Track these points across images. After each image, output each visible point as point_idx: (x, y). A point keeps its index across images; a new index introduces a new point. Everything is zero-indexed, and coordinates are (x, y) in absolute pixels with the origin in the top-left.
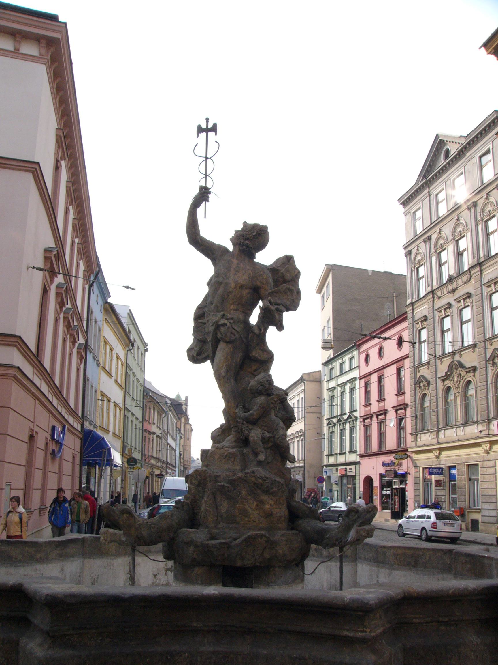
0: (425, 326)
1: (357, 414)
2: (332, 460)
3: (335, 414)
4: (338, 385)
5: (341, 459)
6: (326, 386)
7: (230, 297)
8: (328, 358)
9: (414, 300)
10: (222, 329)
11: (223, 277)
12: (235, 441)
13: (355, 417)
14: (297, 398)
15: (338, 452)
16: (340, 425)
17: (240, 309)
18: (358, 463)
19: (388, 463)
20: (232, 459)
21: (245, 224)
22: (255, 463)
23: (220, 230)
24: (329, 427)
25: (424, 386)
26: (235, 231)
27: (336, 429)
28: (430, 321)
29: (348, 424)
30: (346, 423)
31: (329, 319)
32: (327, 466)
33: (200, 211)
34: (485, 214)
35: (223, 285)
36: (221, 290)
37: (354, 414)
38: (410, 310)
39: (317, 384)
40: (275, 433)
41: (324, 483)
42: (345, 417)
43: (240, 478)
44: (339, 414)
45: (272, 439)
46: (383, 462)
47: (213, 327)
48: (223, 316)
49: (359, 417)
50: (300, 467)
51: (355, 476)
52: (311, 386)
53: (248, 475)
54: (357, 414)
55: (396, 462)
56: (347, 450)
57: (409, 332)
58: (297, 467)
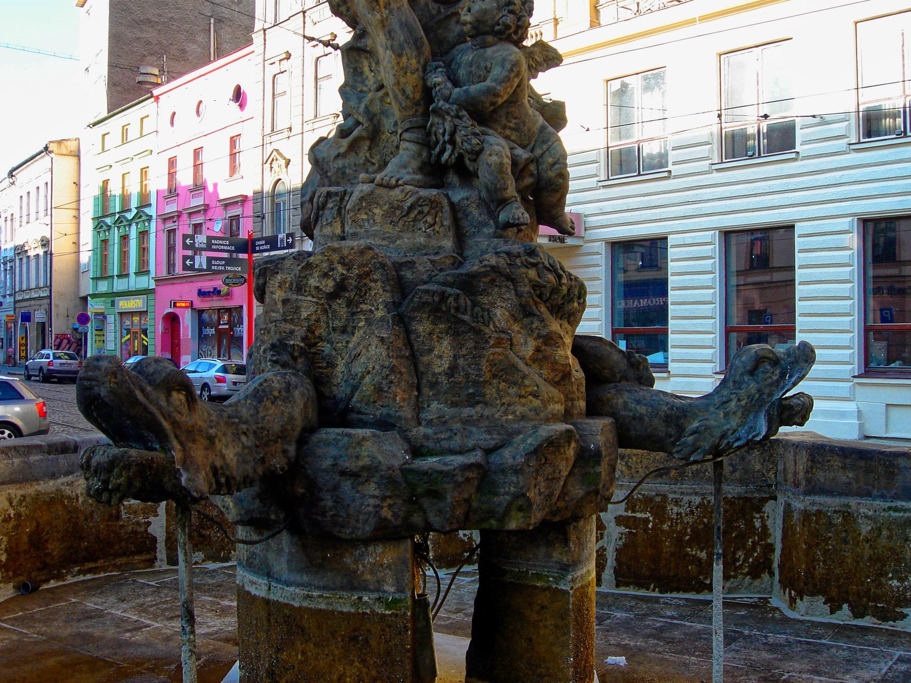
1: (152, 211)
2: (103, 287)
5: (120, 285)
12: (421, 169)
13: (147, 215)
15: (116, 273)
18: (153, 291)
19: (209, 292)
20: (429, 219)
22: (489, 230)
24: (99, 233)
27: (111, 236)
28: (295, 61)
29: (134, 227)
30: (130, 225)
32: (94, 296)
37: (147, 210)
40: (538, 152)
41: (89, 325)
42: (130, 216)
43: (492, 267)
44: (117, 210)
45: (532, 167)
46: (200, 290)
49: (154, 217)
51: (147, 312)
52: (64, 165)
53: (518, 261)
54: (152, 211)
55: (224, 289)
58: (34, 299)
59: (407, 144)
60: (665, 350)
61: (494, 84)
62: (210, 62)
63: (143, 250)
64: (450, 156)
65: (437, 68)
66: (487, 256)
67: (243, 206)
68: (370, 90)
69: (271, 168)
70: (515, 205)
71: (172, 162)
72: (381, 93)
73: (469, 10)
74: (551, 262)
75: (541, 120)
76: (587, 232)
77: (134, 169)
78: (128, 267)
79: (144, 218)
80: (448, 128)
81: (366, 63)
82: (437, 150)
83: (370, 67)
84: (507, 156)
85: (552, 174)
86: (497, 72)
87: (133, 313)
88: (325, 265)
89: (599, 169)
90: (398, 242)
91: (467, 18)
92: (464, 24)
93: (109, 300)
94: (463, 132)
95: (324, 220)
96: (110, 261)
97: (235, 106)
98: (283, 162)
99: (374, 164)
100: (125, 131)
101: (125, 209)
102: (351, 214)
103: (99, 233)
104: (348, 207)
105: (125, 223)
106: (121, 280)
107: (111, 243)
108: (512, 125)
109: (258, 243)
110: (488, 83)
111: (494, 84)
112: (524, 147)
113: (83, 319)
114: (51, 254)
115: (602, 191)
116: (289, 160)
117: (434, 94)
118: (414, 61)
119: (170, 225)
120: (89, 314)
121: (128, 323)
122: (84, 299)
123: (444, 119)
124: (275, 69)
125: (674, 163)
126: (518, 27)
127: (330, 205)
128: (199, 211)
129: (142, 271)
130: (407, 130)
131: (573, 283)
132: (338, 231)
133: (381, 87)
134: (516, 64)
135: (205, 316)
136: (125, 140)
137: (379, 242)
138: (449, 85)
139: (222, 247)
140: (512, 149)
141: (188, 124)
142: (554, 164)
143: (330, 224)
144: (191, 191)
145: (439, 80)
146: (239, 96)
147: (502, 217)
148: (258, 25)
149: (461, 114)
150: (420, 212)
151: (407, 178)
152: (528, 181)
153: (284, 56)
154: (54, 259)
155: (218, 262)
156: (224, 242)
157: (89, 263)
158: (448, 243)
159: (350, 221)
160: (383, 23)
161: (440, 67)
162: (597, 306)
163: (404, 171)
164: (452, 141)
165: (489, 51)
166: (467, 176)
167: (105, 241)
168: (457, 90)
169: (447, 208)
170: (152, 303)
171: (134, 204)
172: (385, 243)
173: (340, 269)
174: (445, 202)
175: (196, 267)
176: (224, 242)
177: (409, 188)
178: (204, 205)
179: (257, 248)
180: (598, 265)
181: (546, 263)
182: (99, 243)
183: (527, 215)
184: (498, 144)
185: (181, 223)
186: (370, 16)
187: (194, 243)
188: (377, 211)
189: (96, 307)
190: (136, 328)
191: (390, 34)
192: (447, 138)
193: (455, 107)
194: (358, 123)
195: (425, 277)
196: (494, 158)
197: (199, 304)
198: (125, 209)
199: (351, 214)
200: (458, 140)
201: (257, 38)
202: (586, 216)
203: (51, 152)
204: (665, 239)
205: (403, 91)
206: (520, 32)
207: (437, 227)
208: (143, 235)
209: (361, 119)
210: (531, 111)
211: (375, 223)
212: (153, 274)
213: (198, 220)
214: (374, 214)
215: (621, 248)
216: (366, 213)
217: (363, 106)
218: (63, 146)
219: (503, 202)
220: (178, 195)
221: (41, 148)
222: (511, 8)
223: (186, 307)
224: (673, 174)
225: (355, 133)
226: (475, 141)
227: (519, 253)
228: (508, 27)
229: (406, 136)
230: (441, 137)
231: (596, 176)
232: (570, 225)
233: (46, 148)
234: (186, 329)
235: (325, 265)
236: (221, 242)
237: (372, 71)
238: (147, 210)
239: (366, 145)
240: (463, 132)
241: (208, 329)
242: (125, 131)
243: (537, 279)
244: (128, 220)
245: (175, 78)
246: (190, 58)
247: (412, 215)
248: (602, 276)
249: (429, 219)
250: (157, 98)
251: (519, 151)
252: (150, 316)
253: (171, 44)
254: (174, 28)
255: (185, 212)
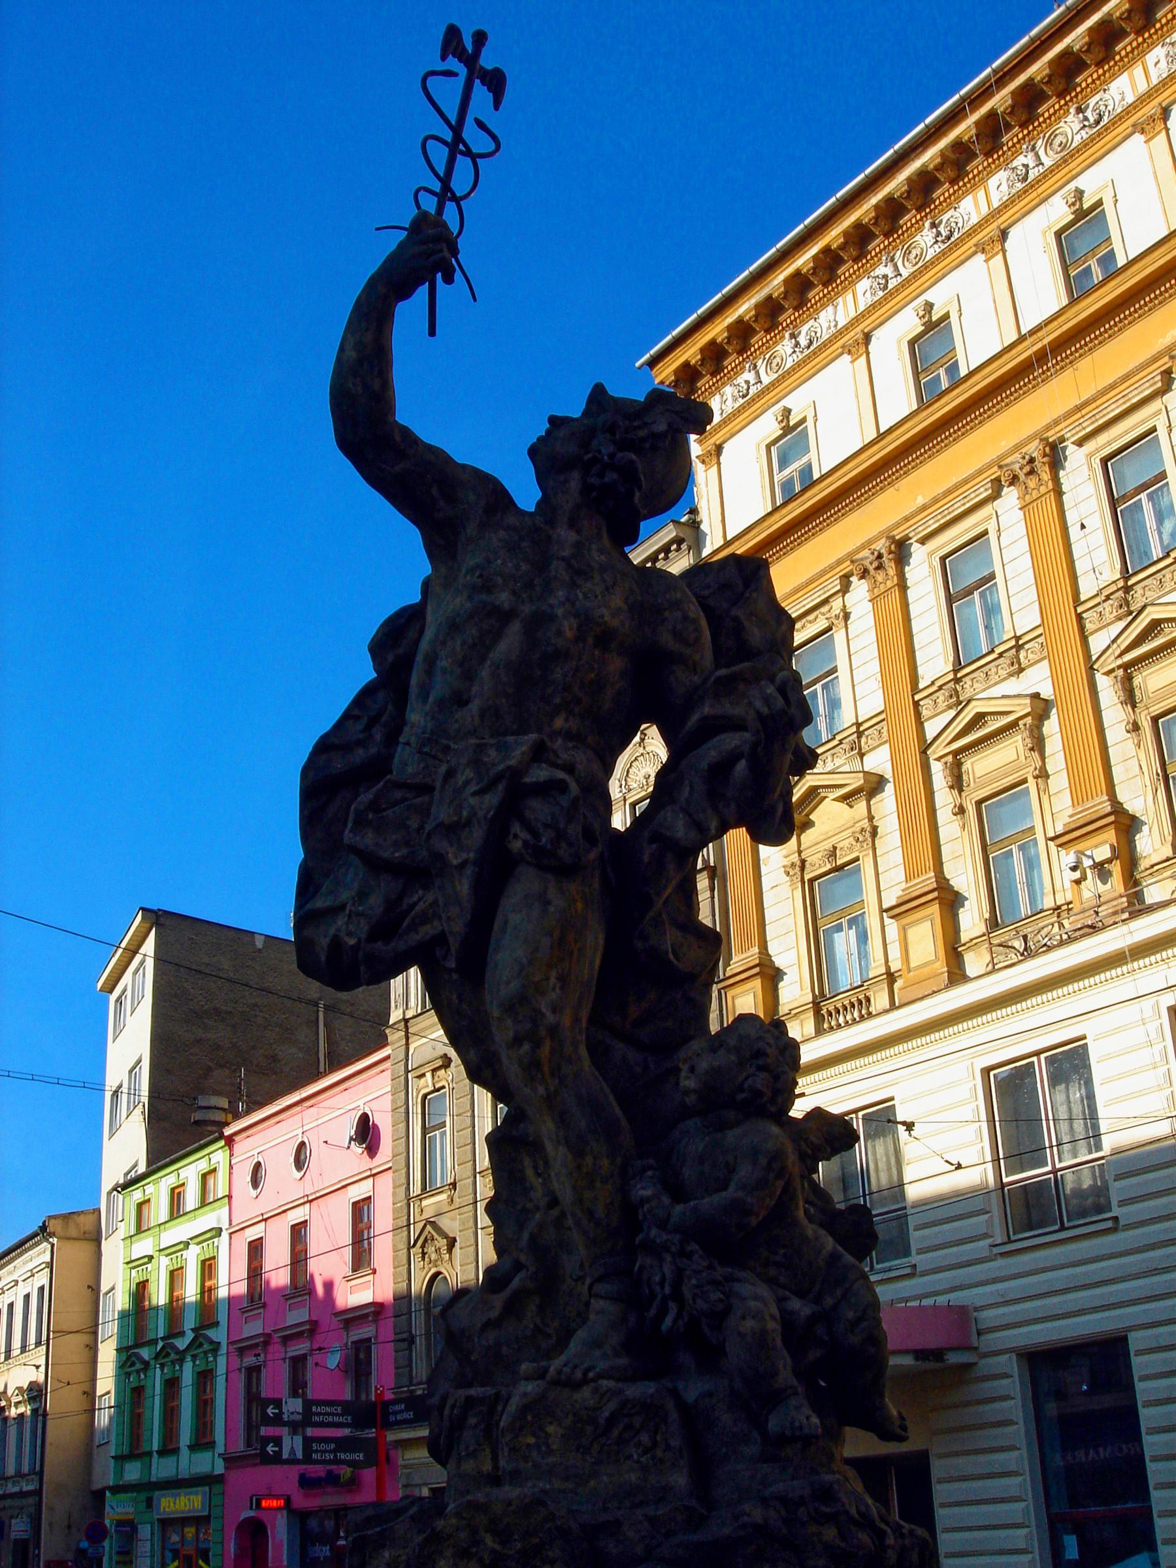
0: (444, 1083)
1: (219, 1334)
2: (133, 1472)
3: (151, 1335)
4: (160, 1251)
5: (162, 1469)
6: (114, 1253)
7: (558, 674)
8: (126, 1174)
9: (409, 1014)
10: (538, 810)
11: (514, 592)
13: (211, 1342)
14: (22, 1289)
15: (155, 1447)
16: (162, 1366)
17: (590, 740)
18: (220, 1479)
20: (645, 1438)
21: (598, 394)
23: (481, 409)
25: (438, 1250)
26: (553, 420)
29: (188, 1367)
30: (181, 1361)
31: (139, 1061)
33: (409, 314)
34: (634, 785)
35: (515, 627)
36: (510, 643)
37: (211, 1333)
38: (399, 1039)
39: (79, 1252)
40: (829, 1301)
41: (106, 1543)
42: (182, 1343)
47: (492, 800)
48: (539, 753)
50: (22, 1494)
51: (209, 1516)
54: (219, 1334)
55: (346, 1472)
56: (185, 1437)
57: (393, 1101)
58: (12, 1496)
59: (601, 1302)
60: (1151, 1546)
61: (740, 1194)
62: (317, 1076)
63: (204, 1406)
64: (675, 1321)
65: (644, 1170)
66: (747, 1507)
67: (376, 1321)
68: (538, 1208)
69: (424, 1254)
70: (793, 1402)
71: (256, 1249)
72: (555, 1212)
73: (692, 1069)
74: (863, 1509)
75: (829, 1243)
76: (982, 1338)
77: (192, 1258)
78: (178, 1436)
79: (206, 1346)
80: (668, 1275)
81: (527, 1162)
82: (653, 1312)
83: (535, 1168)
84: (773, 1317)
85: (855, 1339)
86: (745, 1171)
87: (184, 1521)
88: (463, 1535)
89: (989, 1223)
90: (592, 1483)
91: (688, 1082)
92: (686, 1092)
93: (143, 1496)
94: (694, 1281)
95: (462, 1447)
96: (146, 1425)
97: (358, 1149)
98: (442, 1243)
99: (549, 1336)
100: (176, 1196)
101: (175, 1331)
102: (508, 1437)
103: (128, 1374)
104: (502, 1424)
105: (173, 1356)
106: (163, 1460)
107: (148, 1392)
108: (778, 1258)
109: (392, 1408)
110: (731, 1192)
111: (740, 1194)
112: (801, 1294)
113: (97, 1532)
114: (45, 1414)
115: (1001, 1262)
116: (454, 1240)
117: (641, 1217)
118: (605, 1162)
119: (249, 1360)
120: (107, 1522)
121: (175, 1538)
122: (99, 1496)
123: (661, 1260)
124: (427, 1083)
125: (1122, 1203)
126: (777, 1092)
127: (472, 1421)
128: (302, 1333)
129: (202, 1441)
130: (600, 1279)
131: (907, 1541)
132: (487, 1467)
133: (554, 1202)
134: (777, 1156)
135: (313, 1523)
136: (176, 1209)
137: (558, 1484)
138: (666, 1200)
139: (330, 1419)
140: (780, 1300)
141: (283, 1181)
142: (859, 1320)
143: (473, 1455)
144: (287, 1297)
145: (648, 1193)
146: (366, 1133)
147: (774, 1424)
148: (395, 1016)
149: (689, 1248)
150: (629, 1427)
151: (601, 1366)
152: (814, 1354)
153: (439, 1063)
154: (49, 1423)
155: (323, 1446)
156: (333, 1410)
157: (109, 1429)
158: (680, 1480)
159: (506, 1450)
160: (550, 1100)
161: (650, 1168)
162: (1015, 1474)
163: (597, 1353)
164: (677, 1296)
165: (731, 1136)
166: (710, 1358)
167: (138, 1391)
168: (678, 1208)
169: (674, 1415)
170: (217, 1500)
171: (190, 1322)
172: (570, 1485)
173: (489, 1541)
174: (670, 1405)
175: (285, 1456)
176: (333, 1410)
177: (605, 1383)
178: (310, 1322)
179: (392, 1418)
180: (1007, 1398)
181: (853, 1511)
182: (128, 1391)
183: (815, 1420)
184: (756, 1298)
185: (270, 1357)
186: (527, 1091)
187: (281, 1413)
188: (551, 1429)
189: (120, 1510)
190: (189, 1550)
191: (563, 1119)
192: (667, 1290)
193: (677, 1238)
194: (518, 1266)
195: (639, 1549)
196: (749, 1324)
197: (301, 1501)
198: (175, 1331)
199: (508, 1437)
200: (688, 1295)
201: (395, 1036)
202: (976, 1309)
203: (52, 1235)
204: (1123, 1340)
205: (591, 1213)
206: (780, 1100)
207: (659, 1453)
208: (205, 1378)
209: (523, 1258)
210: (810, 1230)
211: (550, 1452)
212: (220, 1448)
213: (299, 1348)
214: (548, 1436)
215: (1045, 1364)
216: (534, 1434)
217: (526, 1236)
218: (71, 1224)
219: (777, 1398)
220: (264, 1306)
221: (35, 1228)
222: (761, 1062)
223: (279, 1508)
224: (1122, 1223)
225: (516, 1282)
226: (716, 1295)
227: (802, 1497)
228: (758, 1094)
229: (601, 1288)
230: (658, 1289)
231: (986, 1236)
232: (898, 1423)
233: (43, 1228)
234: (278, 1547)
235: (463, 1535)
236: (328, 1409)
237: (539, 1175)
238: (211, 1333)
239: (532, 1308)
240: (694, 1281)
241: (317, 1548)
242: (176, 1196)
243: (838, 1541)
244: (178, 1352)
245: (261, 1105)
246: (287, 1069)
247: (615, 1433)
248: (1018, 1415)
249: (645, 1438)
250: (230, 1141)
251: (795, 1304)
252: (215, 1524)
253: (254, 1047)
254: (259, 1020)
255: (281, 1321)
